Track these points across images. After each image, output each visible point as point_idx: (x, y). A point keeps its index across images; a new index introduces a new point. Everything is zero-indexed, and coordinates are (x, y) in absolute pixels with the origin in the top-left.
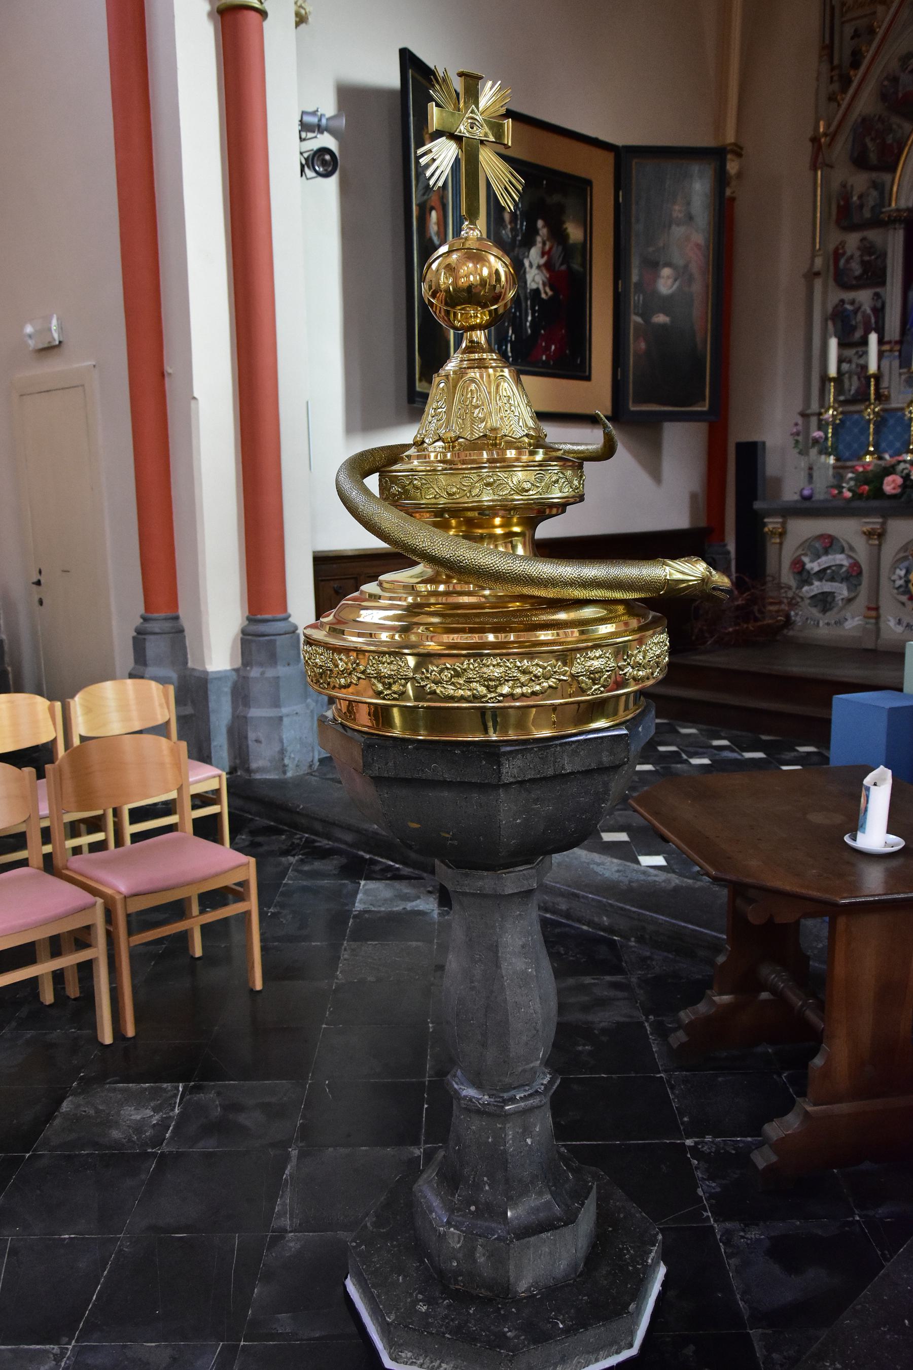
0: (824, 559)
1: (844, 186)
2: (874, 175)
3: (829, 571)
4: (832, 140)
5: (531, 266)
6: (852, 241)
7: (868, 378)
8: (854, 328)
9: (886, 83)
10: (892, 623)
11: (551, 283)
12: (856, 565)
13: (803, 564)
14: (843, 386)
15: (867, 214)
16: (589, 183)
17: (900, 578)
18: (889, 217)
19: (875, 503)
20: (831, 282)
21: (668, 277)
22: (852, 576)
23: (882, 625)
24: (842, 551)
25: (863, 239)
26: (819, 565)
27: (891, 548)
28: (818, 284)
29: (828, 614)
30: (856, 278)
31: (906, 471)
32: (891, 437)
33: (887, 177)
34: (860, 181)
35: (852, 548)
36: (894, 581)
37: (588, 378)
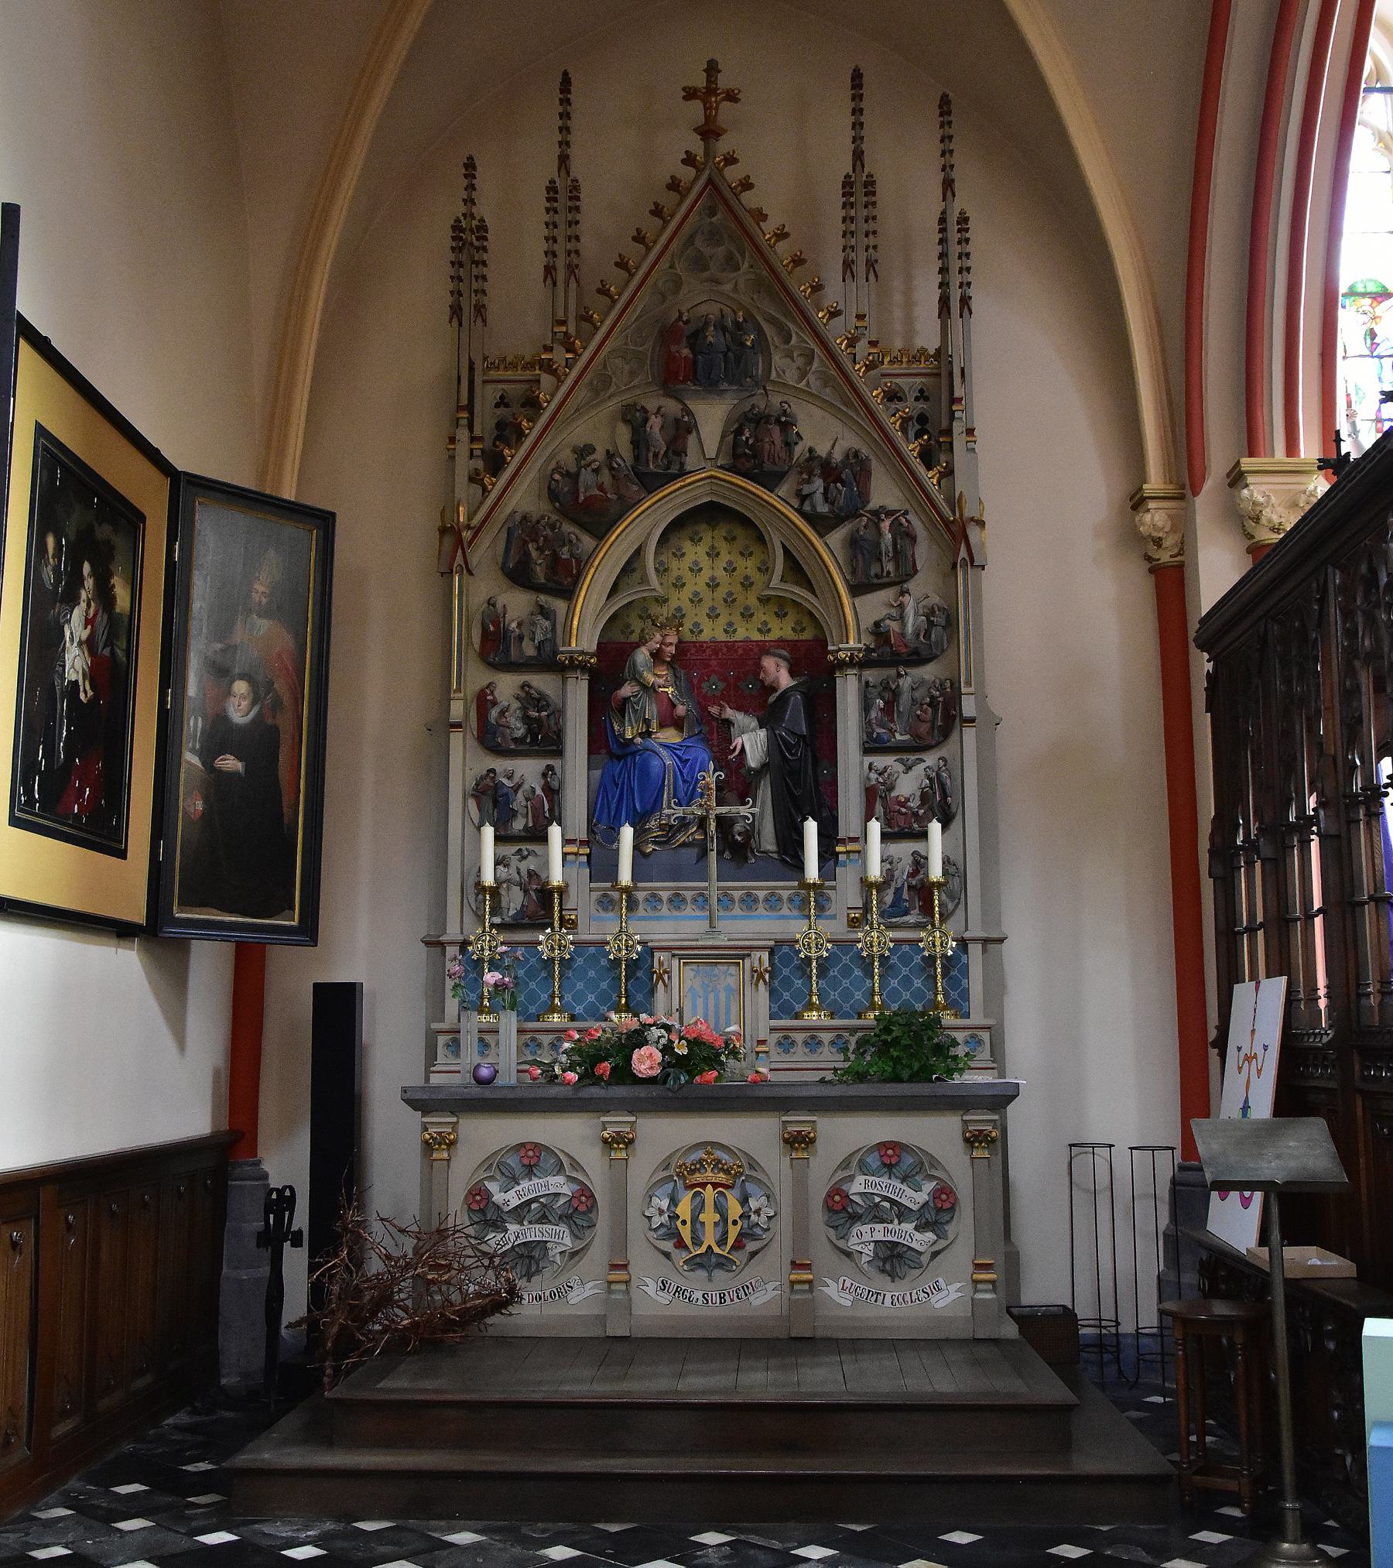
0: (525, 1184)
1: (491, 603)
2: (543, 598)
3: (534, 1206)
4: (475, 536)
5: (72, 639)
6: (507, 686)
7: (551, 892)
8: (514, 814)
9: (557, 477)
10: (651, 1289)
11: (93, 674)
12: (585, 1193)
13: (488, 1195)
14: (500, 902)
15: (529, 650)
16: (333, 515)
17: (661, 1212)
18: (852, 657)
19: (620, 1091)
20: (472, 743)
21: (243, 697)
22: (578, 1212)
23: (635, 1294)
24: (560, 1169)
25: (525, 686)
26: (519, 1196)
27: (642, 1167)
28: (456, 739)
29: (535, 1279)
30: (515, 740)
31: (663, 1041)
32: (580, 985)
33: (559, 606)
34: (517, 604)
35: (576, 1165)
36: (649, 1218)
37: (125, 858)
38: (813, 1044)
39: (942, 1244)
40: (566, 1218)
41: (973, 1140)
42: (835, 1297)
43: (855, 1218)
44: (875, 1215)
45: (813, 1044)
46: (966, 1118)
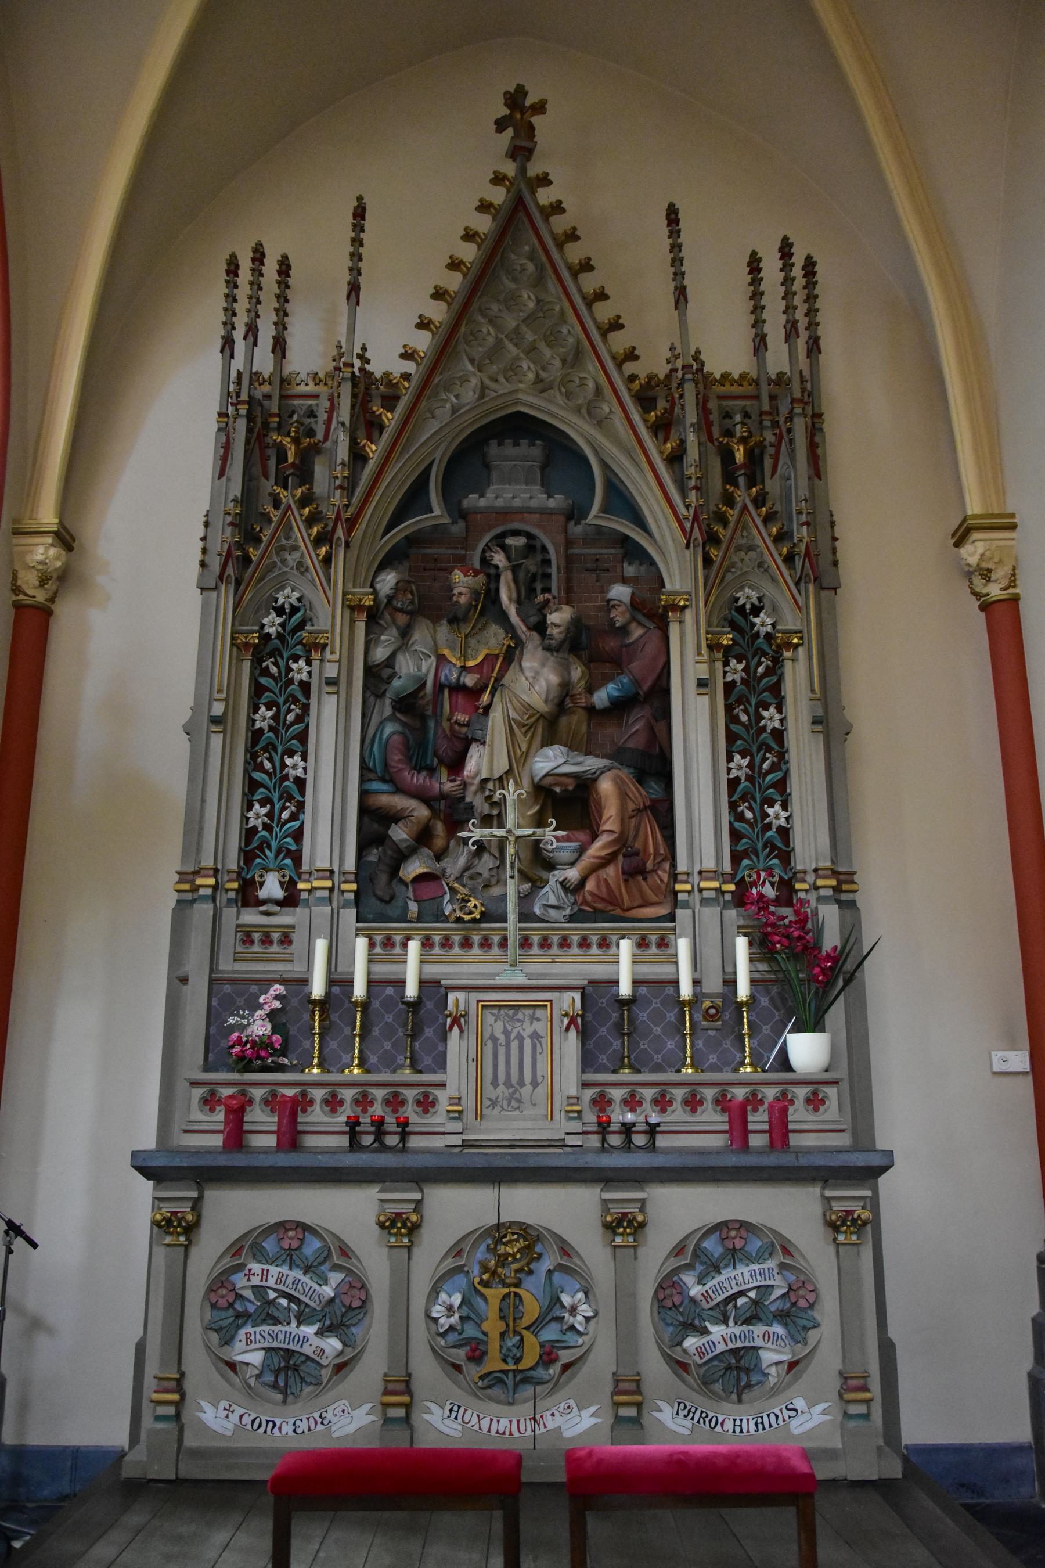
38: (693, 1103)
39: (350, 1353)
40: (782, 1317)
41: (838, 1224)
42: (670, 1424)
43: (243, 1317)
44: (268, 1315)
45: (693, 1103)
46: (828, 1193)
